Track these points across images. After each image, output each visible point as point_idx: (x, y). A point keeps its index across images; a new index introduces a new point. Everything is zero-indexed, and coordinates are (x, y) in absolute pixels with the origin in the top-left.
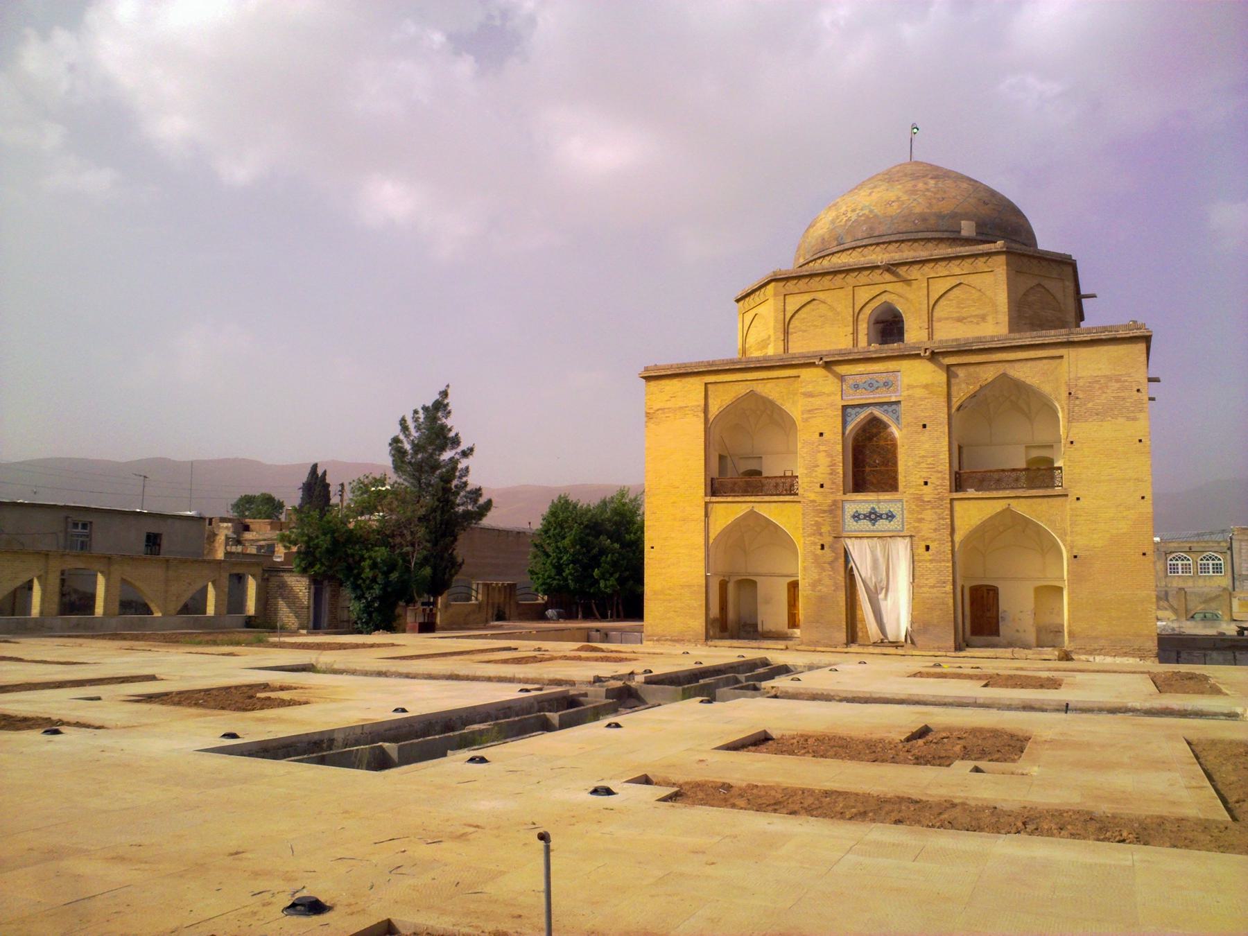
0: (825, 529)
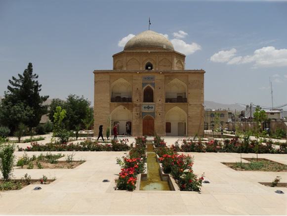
0: (138, 110)
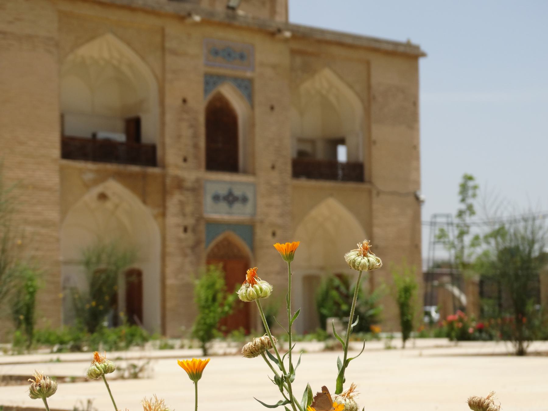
0: (189, 209)
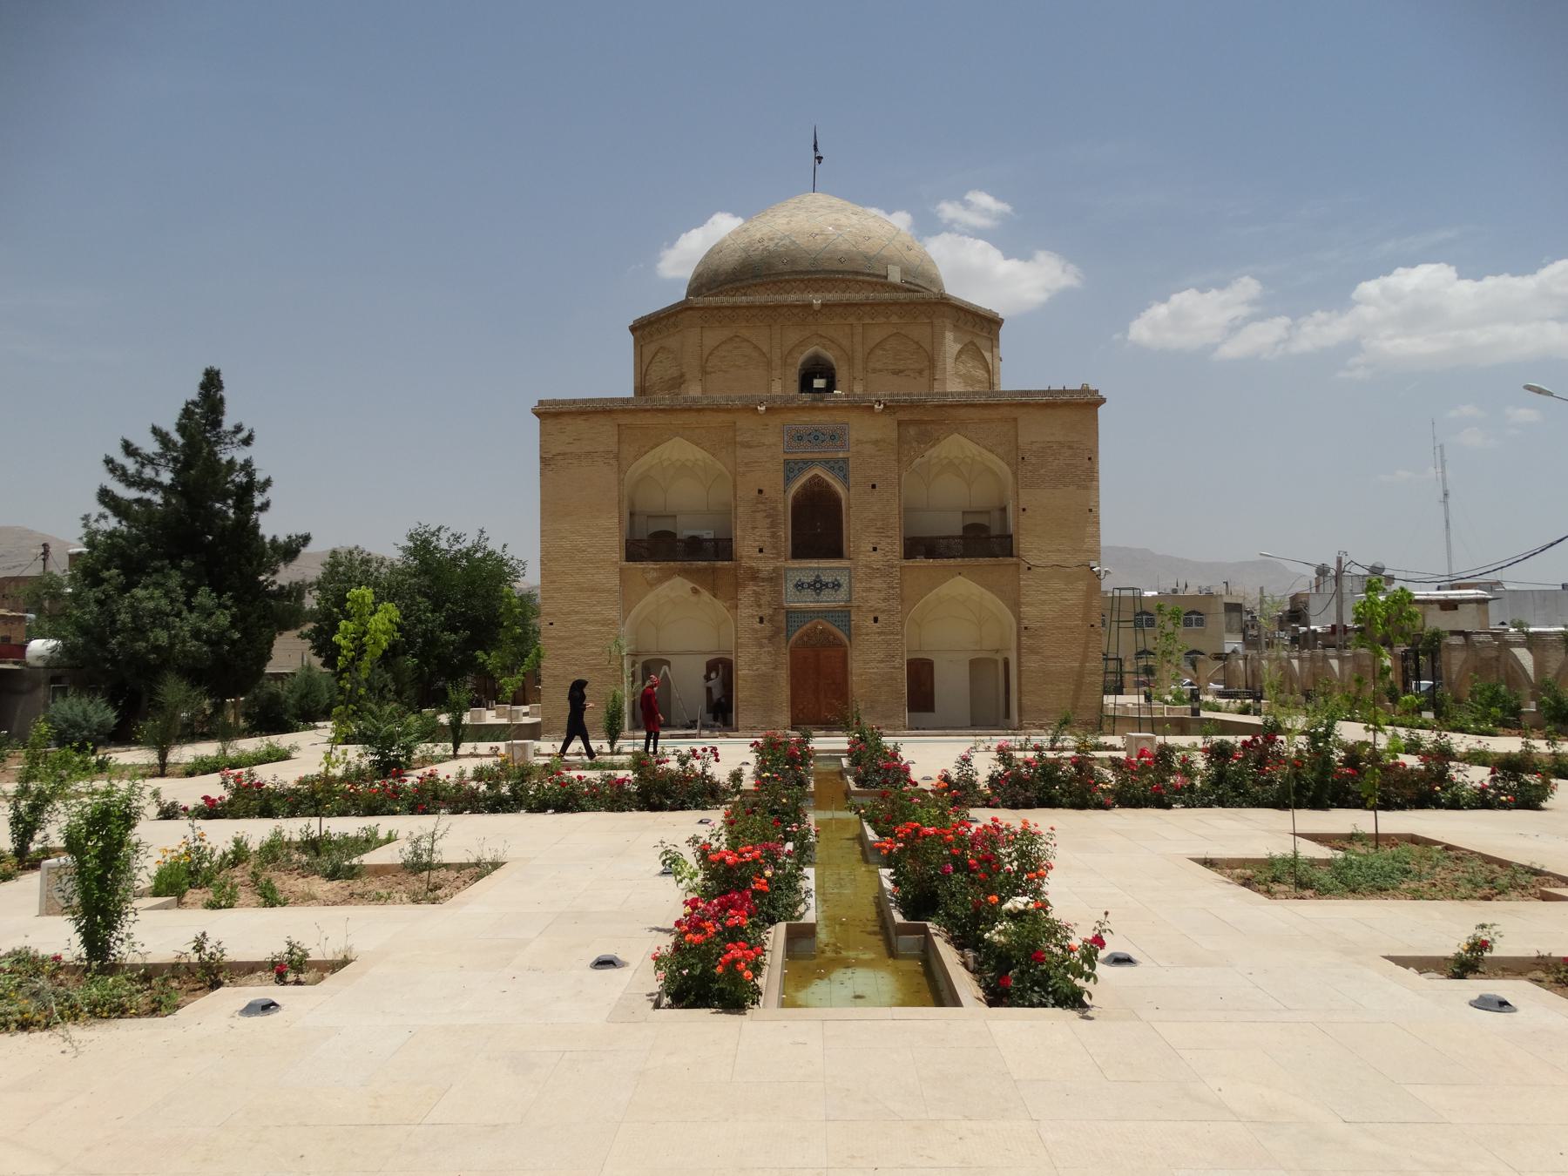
0: (765, 600)
